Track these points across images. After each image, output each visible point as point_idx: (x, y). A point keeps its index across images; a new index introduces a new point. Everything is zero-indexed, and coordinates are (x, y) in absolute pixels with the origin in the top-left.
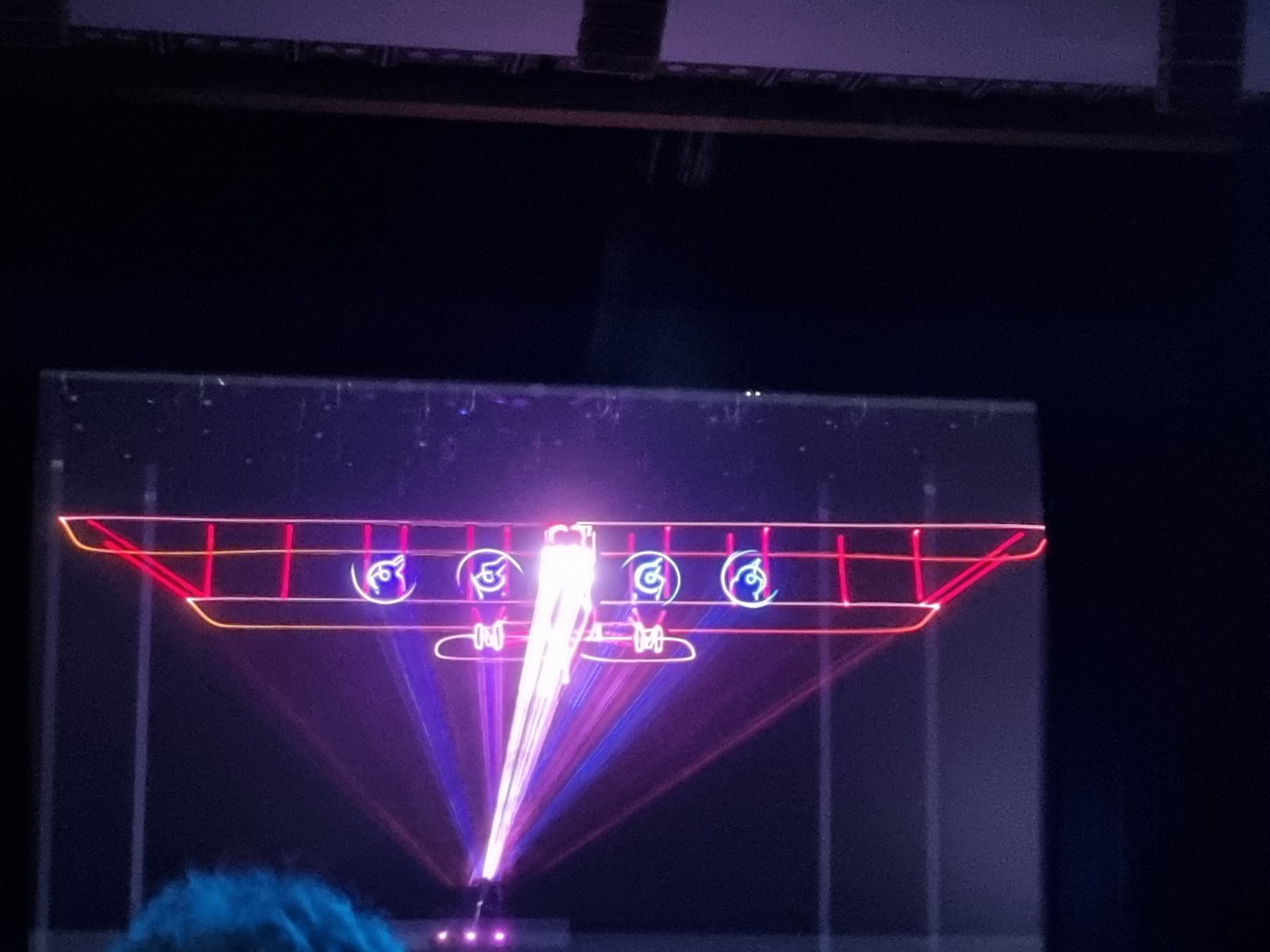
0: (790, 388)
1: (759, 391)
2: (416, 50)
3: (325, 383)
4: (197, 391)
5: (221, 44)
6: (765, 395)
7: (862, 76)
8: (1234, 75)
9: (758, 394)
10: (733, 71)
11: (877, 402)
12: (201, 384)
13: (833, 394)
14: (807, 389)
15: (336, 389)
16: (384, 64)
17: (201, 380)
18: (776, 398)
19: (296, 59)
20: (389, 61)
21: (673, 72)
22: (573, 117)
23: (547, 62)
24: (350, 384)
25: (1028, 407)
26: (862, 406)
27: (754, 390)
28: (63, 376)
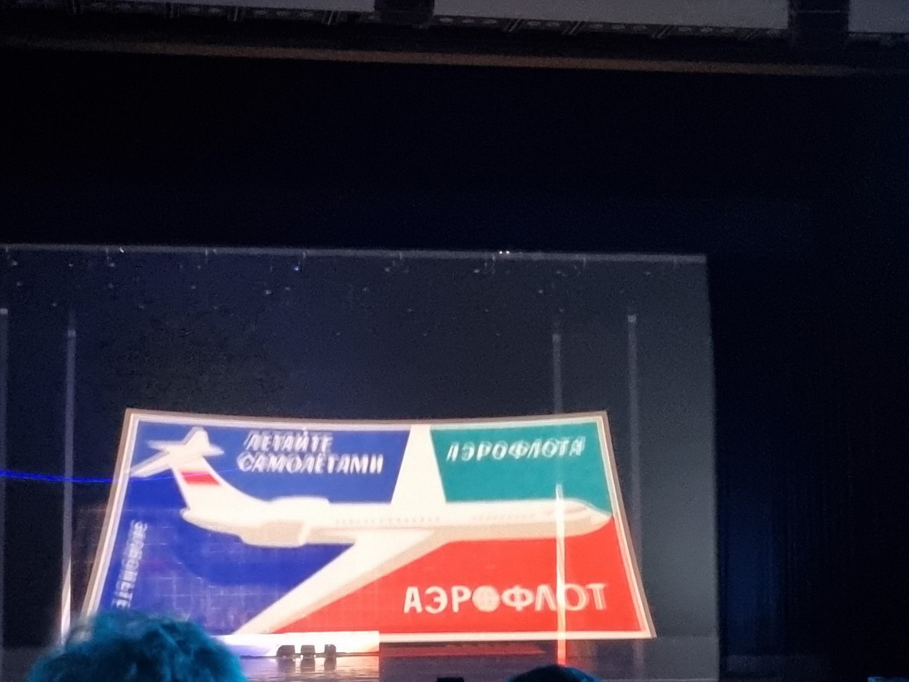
0: (530, 249)
1: (508, 250)
2: (194, 6)
3: (195, 250)
4: (105, 257)
5: (680, 30)
6: (512, 254)
7: (756, 30)
8: (842, 20)
9: (508, 252)
10: (257, 12)
11: (455, 254)
12: (207, 253)
13: (275, 247)
14: (546, 249)
15: (105, 252)
16: (235, 20)
17: (107, 249)
18: (521, 255)
19: (235, 20)
20: (239, 16)
21: (615, 30)
22: (614, 64)
23: (353, 16)
24: (215, 250)
25: (701, 259)
26: (582, 260)
27: (504, 251)
28: (7, 248)
